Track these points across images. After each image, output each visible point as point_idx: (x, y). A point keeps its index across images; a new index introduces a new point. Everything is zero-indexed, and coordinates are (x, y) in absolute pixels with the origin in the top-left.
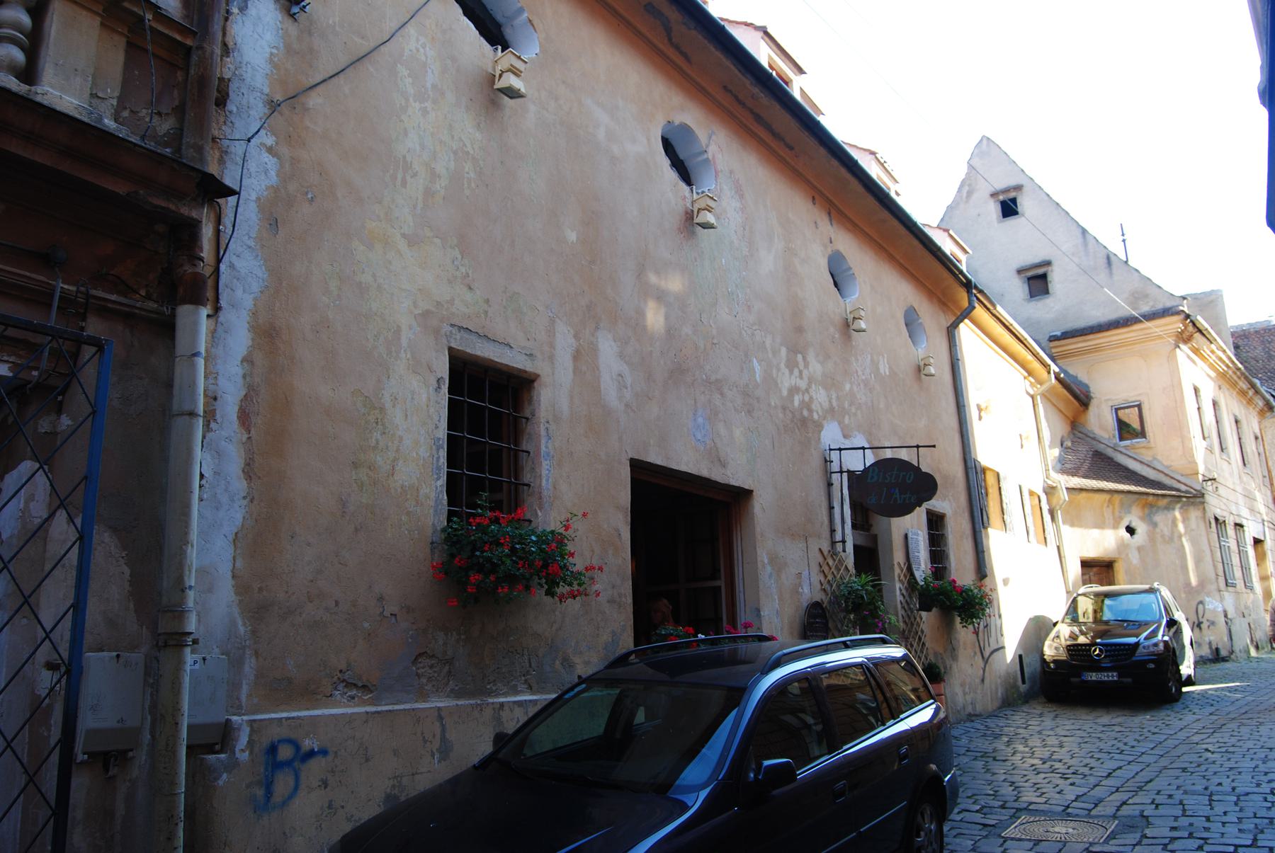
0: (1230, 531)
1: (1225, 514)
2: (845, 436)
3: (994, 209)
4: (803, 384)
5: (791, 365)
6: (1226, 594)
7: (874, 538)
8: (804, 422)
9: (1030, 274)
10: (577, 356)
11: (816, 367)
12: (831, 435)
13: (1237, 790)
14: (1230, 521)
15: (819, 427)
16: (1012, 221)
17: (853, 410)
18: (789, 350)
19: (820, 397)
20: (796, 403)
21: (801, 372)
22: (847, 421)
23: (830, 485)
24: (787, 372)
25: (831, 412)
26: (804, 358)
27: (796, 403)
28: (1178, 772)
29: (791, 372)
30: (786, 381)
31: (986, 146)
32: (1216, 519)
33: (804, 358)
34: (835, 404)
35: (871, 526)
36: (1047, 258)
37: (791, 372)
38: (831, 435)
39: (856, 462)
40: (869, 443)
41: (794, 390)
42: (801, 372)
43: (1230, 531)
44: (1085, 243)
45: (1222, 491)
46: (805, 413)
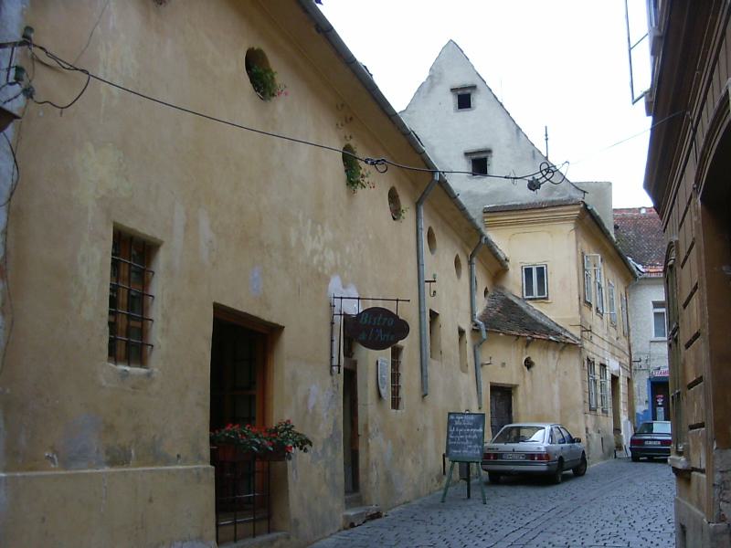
0: (597, 368)
1: (595, 356)
2: (344, 287)
3: (451, 101)
4: (320, 247)
5: (314, 233)
6: (589, 416)
7: (355, 363)
8: (320, 276)
9: (475, 157)
10: (186, 228)
11: (329, 235)
12: (335, 287)
13: (585, 544)
14: (597, 361)
15: (328, 280)
16: (465, 113)
17: (350, 267)
18: (313, 222)
19: (330, 257)
20: (315, 262)
21: (319, 238)
22: (345, 274)
23: (332, 323)
24: (310, 238)
25: (335, 269)
26: (323, 228)
27: (315, 262)
28: (550, 535)
29: (313, 238)
30: (310, 245)
31: (453, 51)
32: (588, 360)
33: (323, 228)
34: (339, 262)
35: (353, 354)
36: (488, 147)
37: (313, 238)
38: (335, 287)
39: (353, 308)
40: (359, 292)
41: (314, 252)
42: (319, 238)
43: (597, 368)
44: (518, 133)
45: (595, 339)
46: (320, 269)
